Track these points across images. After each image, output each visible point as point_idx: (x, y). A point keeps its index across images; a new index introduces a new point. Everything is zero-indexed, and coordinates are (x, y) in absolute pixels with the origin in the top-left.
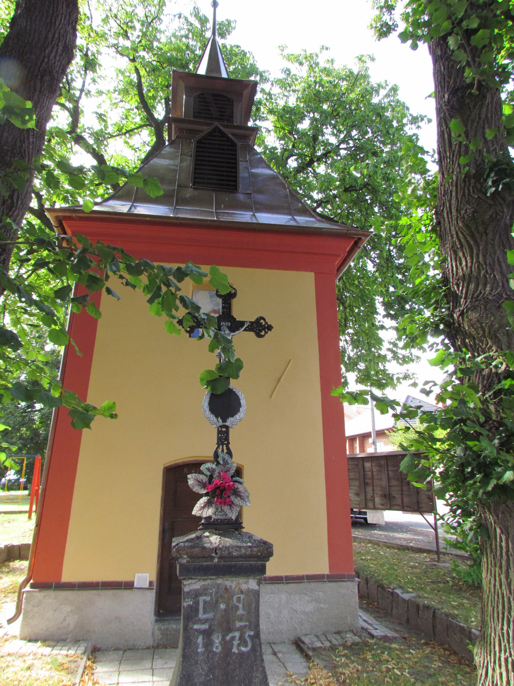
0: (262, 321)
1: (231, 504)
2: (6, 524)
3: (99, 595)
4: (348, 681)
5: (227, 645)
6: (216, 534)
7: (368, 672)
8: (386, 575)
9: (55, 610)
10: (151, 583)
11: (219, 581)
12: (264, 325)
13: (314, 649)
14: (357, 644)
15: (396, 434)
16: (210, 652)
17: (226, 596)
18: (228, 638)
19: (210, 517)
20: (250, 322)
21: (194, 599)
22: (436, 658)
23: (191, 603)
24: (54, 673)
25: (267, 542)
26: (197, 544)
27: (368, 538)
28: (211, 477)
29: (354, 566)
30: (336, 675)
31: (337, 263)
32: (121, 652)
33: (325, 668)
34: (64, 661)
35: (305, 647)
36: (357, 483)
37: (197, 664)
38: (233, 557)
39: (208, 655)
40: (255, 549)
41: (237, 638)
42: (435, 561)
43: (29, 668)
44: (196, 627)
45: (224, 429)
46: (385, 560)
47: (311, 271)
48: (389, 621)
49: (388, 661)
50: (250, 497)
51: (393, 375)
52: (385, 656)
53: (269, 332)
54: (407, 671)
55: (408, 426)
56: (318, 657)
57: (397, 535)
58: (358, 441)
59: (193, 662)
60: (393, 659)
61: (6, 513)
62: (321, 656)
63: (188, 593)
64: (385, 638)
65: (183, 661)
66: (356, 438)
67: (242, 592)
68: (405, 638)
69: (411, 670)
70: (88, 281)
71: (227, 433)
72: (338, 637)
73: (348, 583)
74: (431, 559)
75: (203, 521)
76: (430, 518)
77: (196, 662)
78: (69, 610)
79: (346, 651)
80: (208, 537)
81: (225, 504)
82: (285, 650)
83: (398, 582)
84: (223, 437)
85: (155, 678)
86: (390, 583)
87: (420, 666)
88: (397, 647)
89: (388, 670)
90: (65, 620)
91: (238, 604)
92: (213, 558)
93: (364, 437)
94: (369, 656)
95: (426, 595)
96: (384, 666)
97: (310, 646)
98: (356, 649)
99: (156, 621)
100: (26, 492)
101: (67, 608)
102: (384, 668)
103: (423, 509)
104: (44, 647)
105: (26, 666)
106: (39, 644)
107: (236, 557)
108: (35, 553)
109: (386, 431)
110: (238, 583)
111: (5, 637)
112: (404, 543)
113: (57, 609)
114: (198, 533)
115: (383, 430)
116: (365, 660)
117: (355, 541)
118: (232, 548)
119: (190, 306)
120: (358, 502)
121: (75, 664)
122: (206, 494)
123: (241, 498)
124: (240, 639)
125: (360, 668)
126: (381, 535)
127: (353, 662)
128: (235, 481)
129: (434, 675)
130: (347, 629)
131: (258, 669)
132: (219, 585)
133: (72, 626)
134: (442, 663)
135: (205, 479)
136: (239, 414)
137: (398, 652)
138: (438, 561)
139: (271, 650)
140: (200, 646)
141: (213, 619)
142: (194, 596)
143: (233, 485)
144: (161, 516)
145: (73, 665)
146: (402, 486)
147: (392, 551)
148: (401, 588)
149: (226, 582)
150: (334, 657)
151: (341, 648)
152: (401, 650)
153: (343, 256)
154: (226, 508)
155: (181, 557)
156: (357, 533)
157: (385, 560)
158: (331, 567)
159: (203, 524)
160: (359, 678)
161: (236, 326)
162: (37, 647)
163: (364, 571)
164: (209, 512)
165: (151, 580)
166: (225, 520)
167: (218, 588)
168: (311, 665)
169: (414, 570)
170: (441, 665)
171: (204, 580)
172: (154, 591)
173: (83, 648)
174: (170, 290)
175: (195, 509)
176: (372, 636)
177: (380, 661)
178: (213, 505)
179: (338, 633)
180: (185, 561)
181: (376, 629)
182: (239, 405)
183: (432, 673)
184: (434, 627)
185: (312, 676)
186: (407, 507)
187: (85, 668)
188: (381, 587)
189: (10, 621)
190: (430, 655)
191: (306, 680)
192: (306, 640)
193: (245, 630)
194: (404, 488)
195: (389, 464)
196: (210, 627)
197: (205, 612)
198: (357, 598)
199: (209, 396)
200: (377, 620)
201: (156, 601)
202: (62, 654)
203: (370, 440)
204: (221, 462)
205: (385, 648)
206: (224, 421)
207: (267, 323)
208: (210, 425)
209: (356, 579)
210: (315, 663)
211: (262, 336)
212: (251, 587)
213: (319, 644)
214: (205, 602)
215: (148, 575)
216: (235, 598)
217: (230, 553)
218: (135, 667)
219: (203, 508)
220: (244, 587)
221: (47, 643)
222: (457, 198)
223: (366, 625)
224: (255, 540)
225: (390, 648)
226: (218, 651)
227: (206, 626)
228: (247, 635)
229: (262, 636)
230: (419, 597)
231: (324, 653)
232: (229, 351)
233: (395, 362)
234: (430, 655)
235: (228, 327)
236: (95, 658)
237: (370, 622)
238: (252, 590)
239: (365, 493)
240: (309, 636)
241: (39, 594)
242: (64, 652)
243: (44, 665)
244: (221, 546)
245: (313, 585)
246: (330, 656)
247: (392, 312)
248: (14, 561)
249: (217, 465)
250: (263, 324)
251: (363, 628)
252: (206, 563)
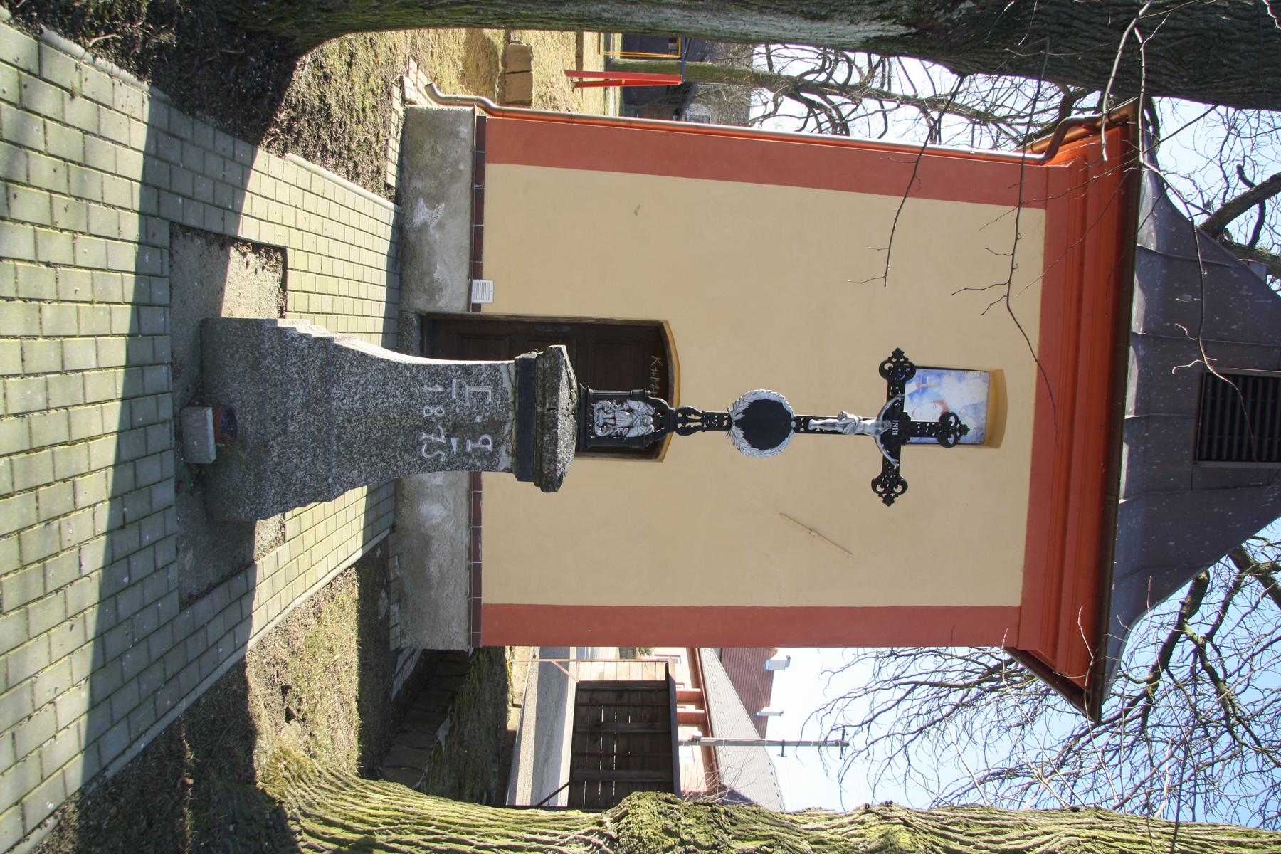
5: (428, 425)
10: (477, 307)
47: (1023, 600)
66: (702, 708)
71: (720, 428)
76: (563, 799)
84: (713, 422)
144: (581, 319)
206: (738, 423)
207: (896, 495)
222: (1117, 840)
235: (890, 431)
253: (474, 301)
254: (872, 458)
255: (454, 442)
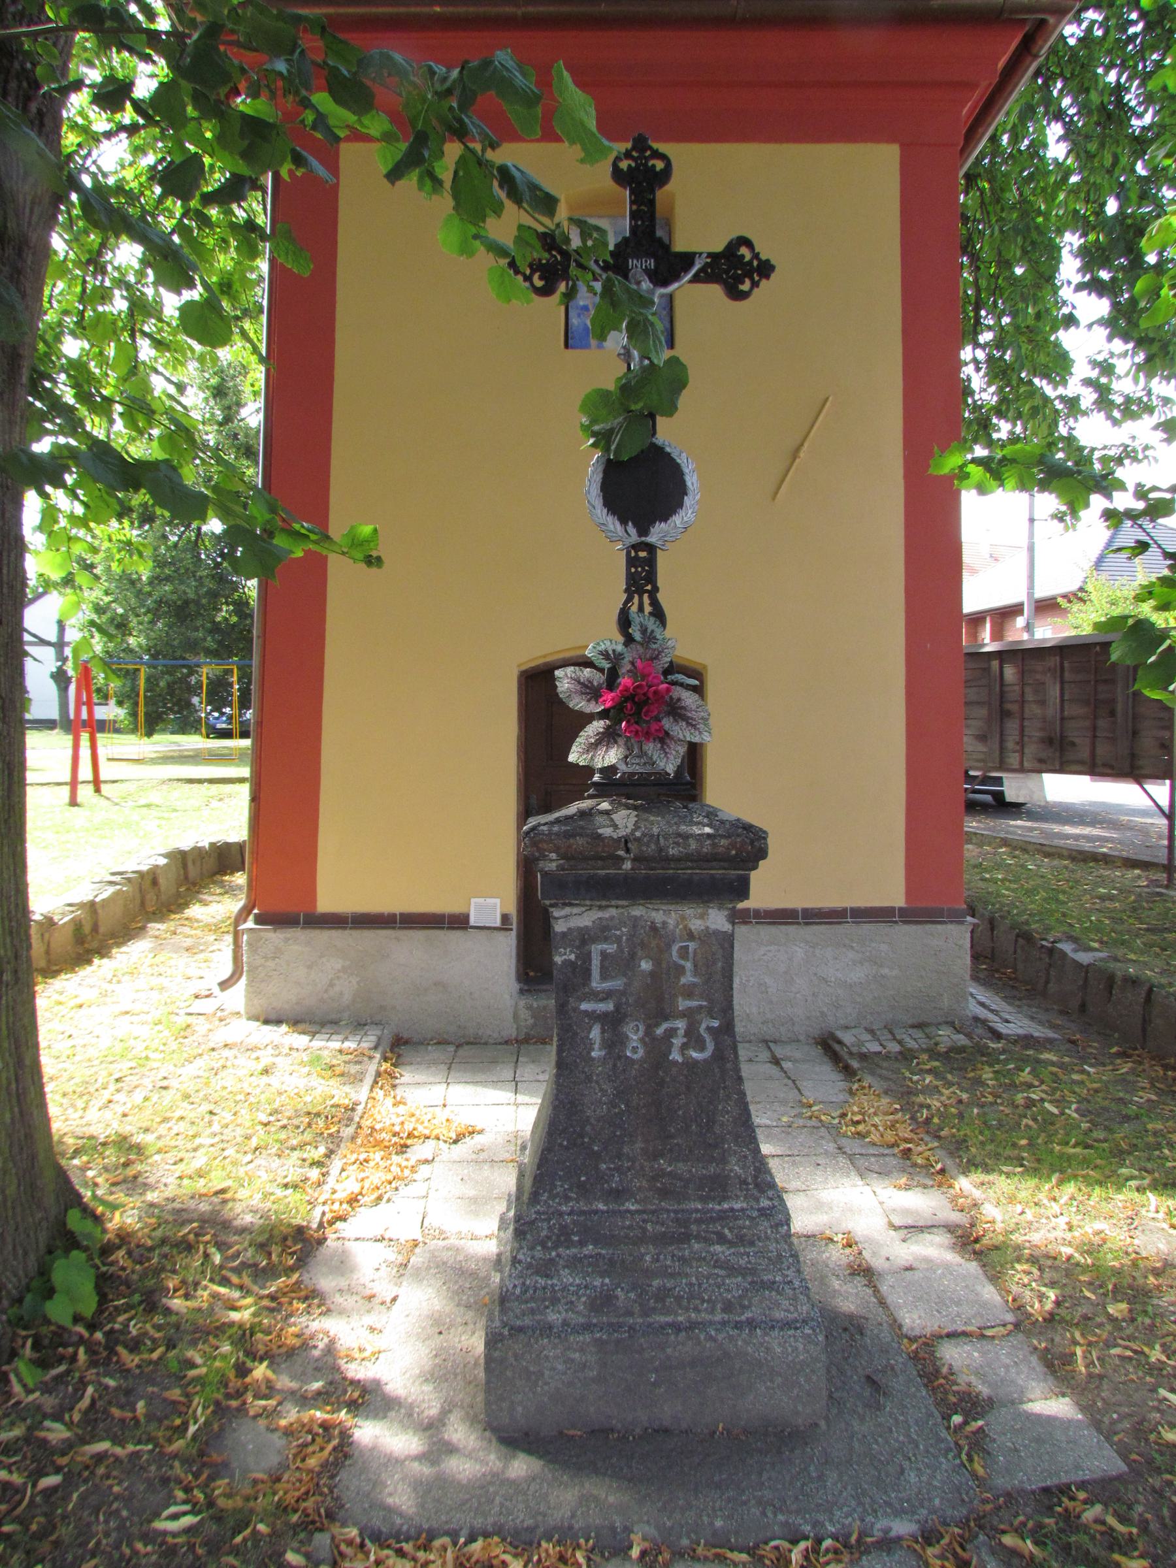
0: (744, 251)
1: (664, 738)
2: (215, 804)
3: (398, 939)
4: (936, 1120)
5: (658, 1047)
6: (628, 807)
7: (982, 1106)
8: (1040, 913)
9: (310, 967)
10: (505, 918)
11: (637, 911)
12: (750, 263)
13: (863, 1057)
14: (962, 1050)
15: (1084, 608)
16: (620, 1057)
17: (654, 944)
18: (659, 1031)
19: (612, 769)
20: (710, 255)
21: (578, 948)
22: (1145, 1083)
23: (573, 957)
24: (315, 1081)
25: (751, 826)
26: (582, 828)
27: (1002, 835)
28: (612, 676)
29: (966, 894)
30: (910, 1108)
31: (966, 110)
32: (452, 1048)
33: (886, 1093)
34: (335, 1062)
35: (843, 1052)
36: (983, 712)
37: (590, 1081)
38: (668, 859)
39: (615, 1065)
40: (723, 842)
41: (681, 1032)
42: (1161, 886)
43: (266, 1071)
44: (584, 1006)
45: (643, 554)
46: (1039, 881)
47: (890, 140)
48: (1039, 1007)
49: (1030, 1086)
50: (711, 721)
51: (1093, 450)
52: (1026, 1075)
53: (764, 282)
54: (1074, 1106)
55: (1146, 539)
56: (873, 1074)
57: (1069, 830)
58: (988, 625)
59: (583, 1076)
60: (1042, 1082)
61: (212, 781)
62: (879, 1071)
63: (564, 934)
64: (1027, 1041)
65: (558, 1076)
66: (984, 619)
67: (691, 936)
68: (1073, 1042)
69: (1084, 1106)
70: (242, 135)
71: (651, 562)
72: (918, 1034)
73: (950, 927)
74: (1152, 881)
75: (596, 778)
77: (589, 1079)
78: (339, 966)
79: (937, 1064)
80: (607, 813)
81: (648, 735)
82: (798, 1055)
83: (1066, 929)
84: (642, 574)
85: (521, 1098)
86: (1048, 929)
87: (1105, 1099)
88: (1055, 1059)
89: (1030, 1103)
90: (331, 985)
91: (682, 962)
92: (622, 859)
93: (1005, 615)
94: (987, 1074)
95: (1132, 956)
96: (1020, 1096)
97: (854, 1050)
98: (958, 1061)
99: (522, 992)
100: (247, 743)
101: (336, 964)
102: (1020, 1098)
103: (1143, 772)
104: (296, 1035)
105: (260, 1067)
106: (284, 1028)
107: (678, 860)
108: (256, 853)
109: (1059, 600)
110: (683, 918)
111: (219, 1014)
112: (1087, 846)
113: (312, 964)
114: (585, 804)
115: (1054, 598)
116: (978, 1082)
117: (969, 842)
118: (666, 839)
119: (527, 195)
120: (982, 756)
121: (358, 1067)
122: (604, 715)
123: (689, 724)
124: (687, 1034)
125: (965, 1096)
126: (1031, 829)
127: (950, 1084)
128: (674, 683)
129: (1137, 1117)
130: (940, 1020)
131: (729, 1097)
132: (636, 919)
133: (347, 998)
134: (1156, 1094)
135: (598, 678)
136: (682, 513)
137: (1054, 1069)
138: (1167, 887)
139: (768, 1054)
140: (596, 1046)
141: (623, 993)
142: (577, 943)
143: (668, 690)
144: (519, 780)
145: (354, 1069)
146: (1095, 718)
147: (1056, 862)
148: (1074, 939)
149: (654, 914)
150: (907, 1074)
151: (925, 1057)
152: (1061, 1066)
153: (986, 85)
154: (651, 748)
155: (544, 857)
156: (973, 824)
157: (1039, 881)
158: (907, 901)
159: (595, 784)
160: (961, 1116)
161: (671, 266)
162: (281, 1034)
163: (986, 903)
164: (611, 756)
165: (506, 911)
166: (650, 774)
167: (635, 926)
168: (856, 1086)
169: (1107, 904)
170: (1154, 1097)
171: (600, 908)
172: (514, 933)
173: (374, 1038)
174: (472, 151)
175: (574, 748)
176: (997, 1036)
177: (1013, 1085)
178: (621, 741)
179: (920, 1026)
180: (553, 866)
181: (1007, 1021)
182: (682, 490)
183: (1130, 1112)
184: (1145, 1021)
185: (855, 1109)
186: (1104, 765)
187: (378, 1074)
188: (1026, 937)
189: (224, 985)
190: (1130, 1078)
191: (843, 1115)
192: (847, 1038)
193: (698, 1017)
194: (1101, 723)
195: (1066, 664)
196: (617, 1007)
197: (604, 977)
198: (968, 958)
199: (601, 469)
200: (1009, 1004)
201: (518, 955)
202: (329, 1046)
203: (1020, 622)
204: (638, 636)
205: (1025, 1060)
206: (643, 531)
207: (756, 256)
208: (606, 544)
209: (969, 918)
210: (865, 1084)
211: (743, 296)
212: (713, 927)
213: (874, 1047)
214: (604, 955)
215: (498, 901)
216: (675, 949)
217: (661, 850)
218: (480, 1077)
219: (593, 747)
220: (696, 925)
221: (301, 1027)
223: (983, 1013)
224: (722, 822)
225: (1038, 1061)
226: (635, 1057)
227: (609, 1006)
228: (703, 1026)
229: (739, 1028)
230: (1116, 959)
231: (885, 1064)
232: (646, 333)
233: (1099, 417)
234: (1130, 1078)
235: (647, 271)
236: (399, 1056)
237: (994, 1007)
238: (717, 933)
239: (1002, 735)
240: (854, 1031)
241: (274, 937)
242: (335, 1045)
243: (296, 1067)
244: (638, 834)
245: (867, 929)
246: (897, 1072)
247: (1104, 275)
248: (232, 873)
249: (626, 644)
250: (748, 257)
251: (976, 1019)
252: (602, 872)
253: (498, 923)
254: (696, 302)
255: (683, 1004)
